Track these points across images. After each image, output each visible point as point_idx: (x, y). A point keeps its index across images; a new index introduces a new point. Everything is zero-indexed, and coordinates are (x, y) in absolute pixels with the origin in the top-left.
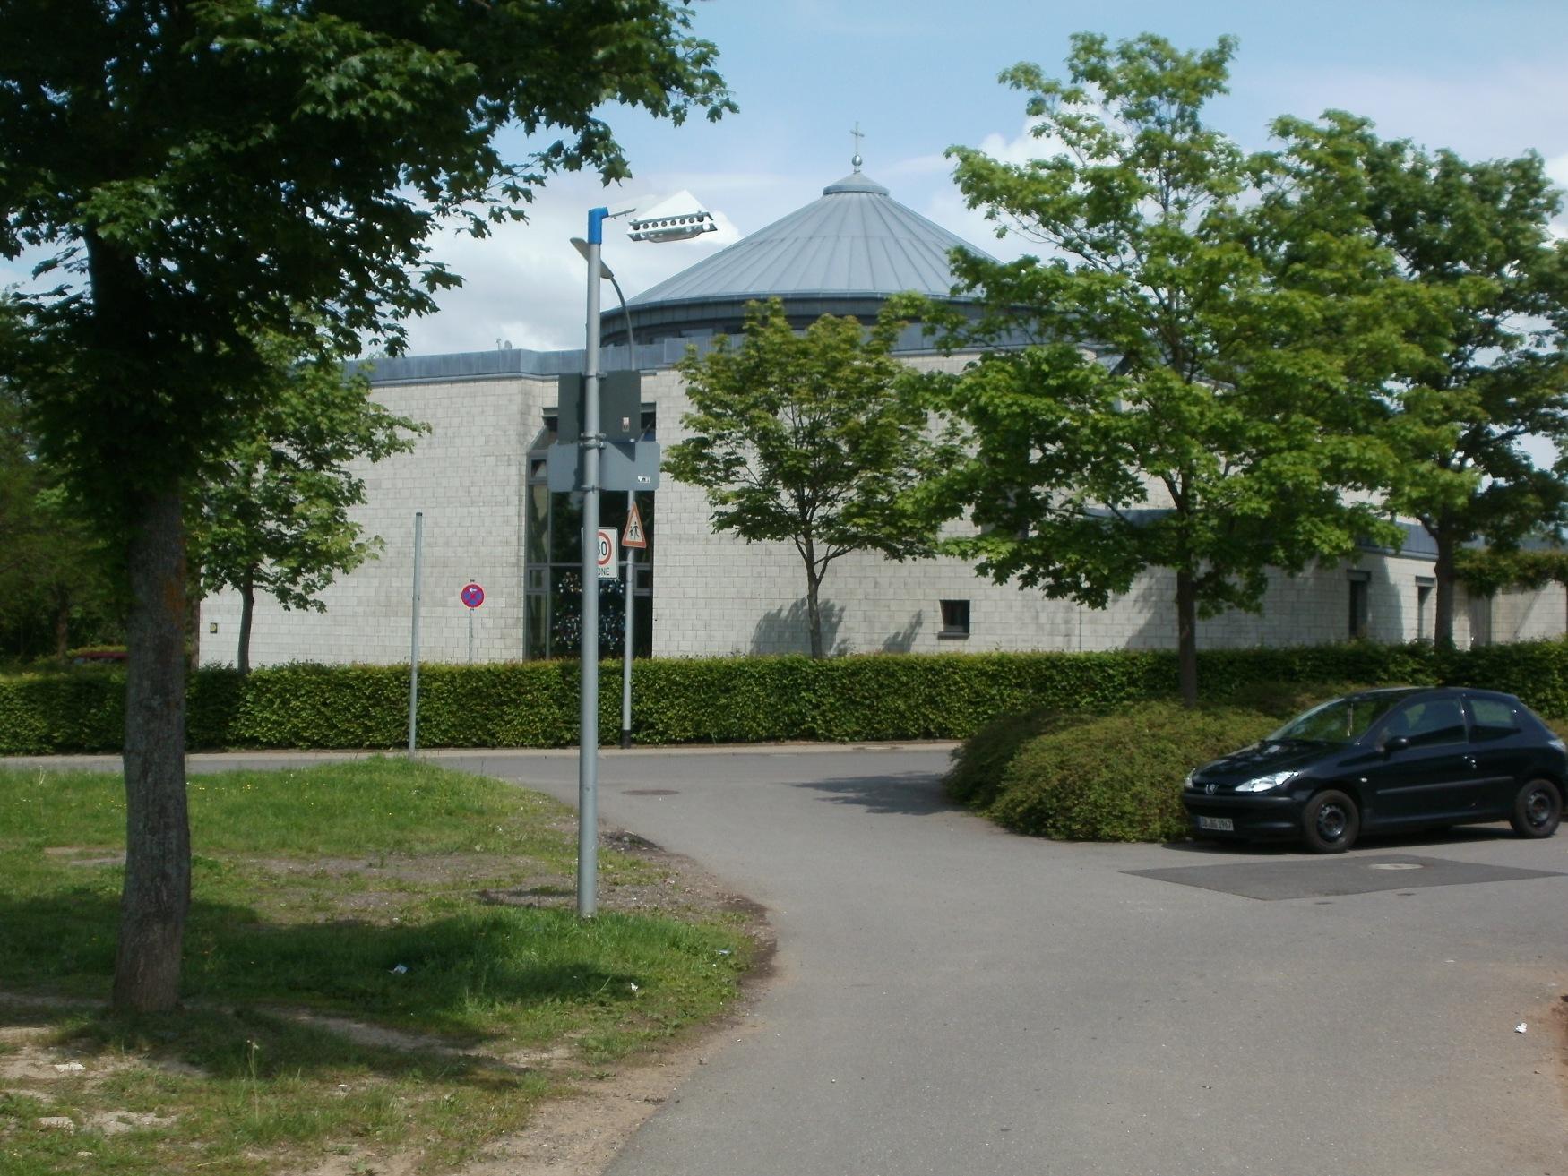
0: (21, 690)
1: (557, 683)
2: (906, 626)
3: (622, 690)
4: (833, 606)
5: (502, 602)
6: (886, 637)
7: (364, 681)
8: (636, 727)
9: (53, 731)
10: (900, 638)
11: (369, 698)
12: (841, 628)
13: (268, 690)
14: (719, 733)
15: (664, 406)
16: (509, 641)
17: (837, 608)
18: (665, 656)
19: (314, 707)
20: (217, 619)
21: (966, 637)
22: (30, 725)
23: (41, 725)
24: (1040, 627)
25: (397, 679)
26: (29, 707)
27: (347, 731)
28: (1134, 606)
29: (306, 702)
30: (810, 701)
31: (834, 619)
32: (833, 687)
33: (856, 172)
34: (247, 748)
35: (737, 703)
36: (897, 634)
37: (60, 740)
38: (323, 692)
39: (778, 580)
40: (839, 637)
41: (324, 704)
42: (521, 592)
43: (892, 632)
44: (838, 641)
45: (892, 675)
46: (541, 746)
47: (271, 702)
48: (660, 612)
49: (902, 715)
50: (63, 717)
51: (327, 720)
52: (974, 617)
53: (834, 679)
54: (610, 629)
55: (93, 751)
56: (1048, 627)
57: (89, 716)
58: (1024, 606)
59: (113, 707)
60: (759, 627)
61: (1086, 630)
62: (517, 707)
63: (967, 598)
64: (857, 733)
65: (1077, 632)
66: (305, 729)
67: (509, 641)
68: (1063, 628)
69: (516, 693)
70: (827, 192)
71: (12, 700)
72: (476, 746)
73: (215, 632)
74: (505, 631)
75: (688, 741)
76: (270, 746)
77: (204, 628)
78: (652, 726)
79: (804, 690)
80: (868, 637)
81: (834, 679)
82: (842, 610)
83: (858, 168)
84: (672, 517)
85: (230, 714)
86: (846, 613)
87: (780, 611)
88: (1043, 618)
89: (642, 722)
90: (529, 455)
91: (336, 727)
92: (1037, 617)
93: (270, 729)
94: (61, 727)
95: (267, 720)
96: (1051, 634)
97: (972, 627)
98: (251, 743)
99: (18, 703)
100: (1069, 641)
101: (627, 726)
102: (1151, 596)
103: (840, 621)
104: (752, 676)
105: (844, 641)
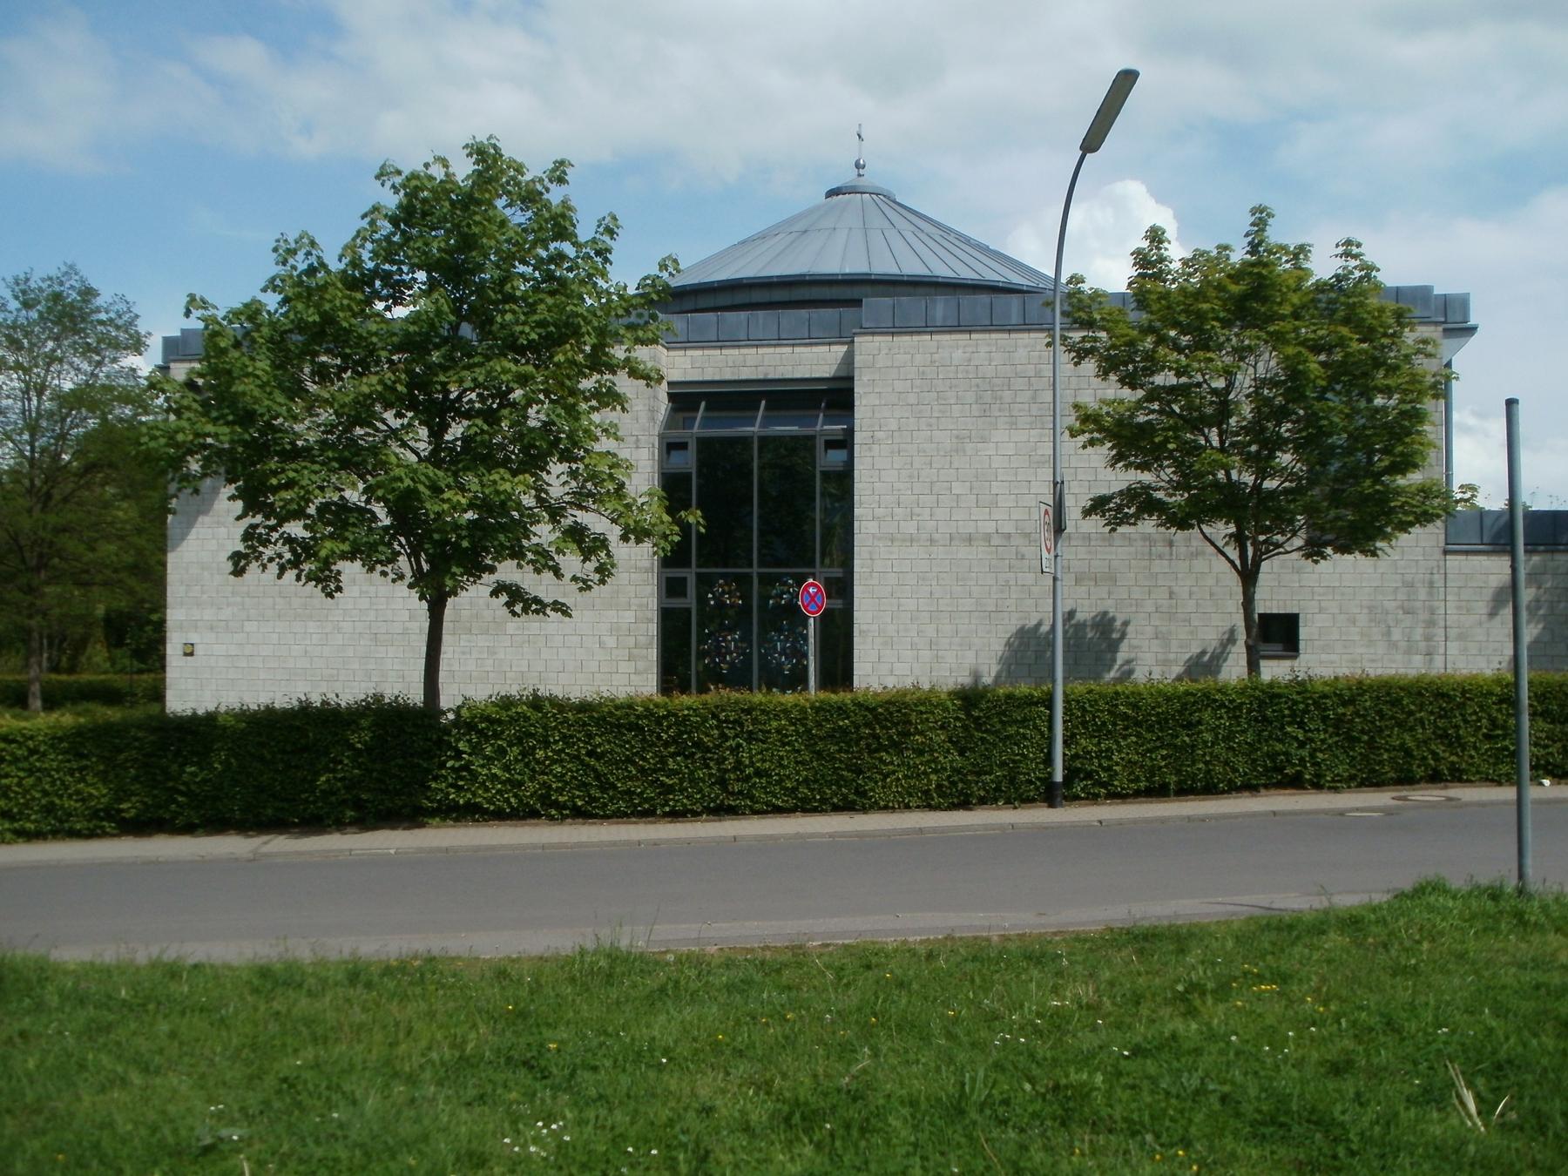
0: (61, 739)
1: (958, 719)
2: (1215, 644)
3: (1051, 728)
4: (1113, 619)
5: (629, 616)
6: (1187, 656)
7: (659, 722)
8: (1071, 774)
9: (121, 801)
10: (1206, 658)
11: (666, 744)
12: (1124, 646)
13: (497, 736)
14: (1179, 783)
15: (865, 379)
16: (641, 665)
17: (1118, 623)
18: (876, 687)
19: (577, 757)
20: (193, 638)
21: (1295, 657)
22: (78, 792)
23: (99, 792)
24: (1393, 645)
25: (715, 716)
26: (75, 765)
27: (629, 792)
28: (1493, 614)
29: (562, 750)
30: (1296, 738)
31: (1115, 636)
32: (1325, 719)
33: (859, 175)
34: (456, 820)
35: (1205, 742)
36: (1203, 653)
37: (133, 812)
38: (590, 736)
39: (1033, 588)
40: (1121, 657)
41: (590, 754)
42: (653, 604)
43: (1196, 650)
44: (1119, 662)
45: (1396, 703)
46: (937, 808)
47: (502, 752)
48: (864, 627)
49: (1408, 753)
50: (136, 779)
51: (598, 777)
52: (1304, 633)
53: (1326, 709)
54: (784, 649)
55: (189, 829)
56: (1403, 644)
57: (185, 777)
58: (1371, 621)
59: (227, 764)
60: (1008, 644)
61: (1453, 648)
62: (900, 752)
63: (1295, 611)
64: (1352, 778)
65: (1442, 651)
66: (560, 791)
67: (641, 665)
68: (1422, 645)
69: (899, 734)
70: (832, 193)
71: (44, 754)
72: (837, 809)
73: (191, 654)
74: (635, 651)
75: (1138, 794)
76: (499, 816)
77: (173, 649)
78: (1089, 775)
79: (1290, 724)
80: (1160, 657)
81: (1326, 709)
82: (1126, 624)
83: (861, 171)
84: (880, 512)
85: (428, 771)
86: (1130, 629)
87: (1039, 624)
88: (1396, 635)
89: (1078, 770)
90: (661, 437)
91: (614, 787)
92: (1389, 633)
93: (499, 792)
94: (133, 794)
95: (494, 777)
96: (1408, 652)
97: (1302, 645)
98: (470, 813)
99: (53, 761)
100: (1431, 661)
101: (1059, 777)
102: (1539, 608)
103: (1123, 636)
104: (1223, 705)
105: (1128, 662)
